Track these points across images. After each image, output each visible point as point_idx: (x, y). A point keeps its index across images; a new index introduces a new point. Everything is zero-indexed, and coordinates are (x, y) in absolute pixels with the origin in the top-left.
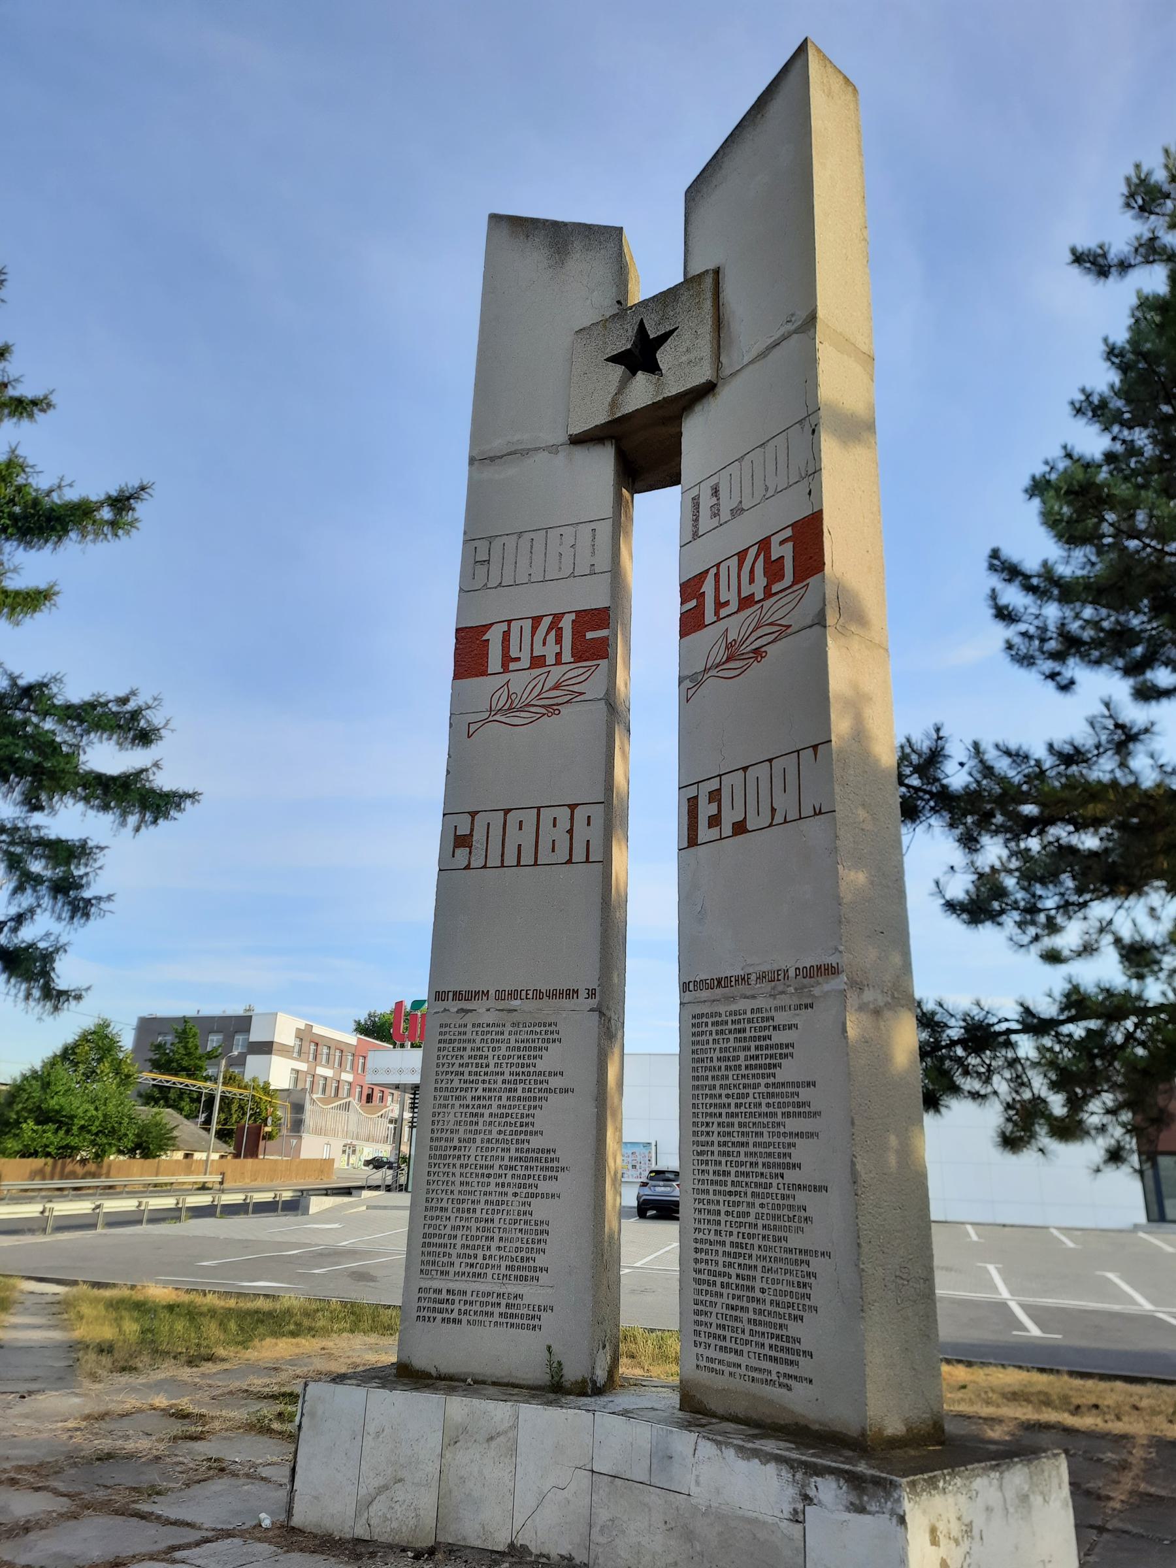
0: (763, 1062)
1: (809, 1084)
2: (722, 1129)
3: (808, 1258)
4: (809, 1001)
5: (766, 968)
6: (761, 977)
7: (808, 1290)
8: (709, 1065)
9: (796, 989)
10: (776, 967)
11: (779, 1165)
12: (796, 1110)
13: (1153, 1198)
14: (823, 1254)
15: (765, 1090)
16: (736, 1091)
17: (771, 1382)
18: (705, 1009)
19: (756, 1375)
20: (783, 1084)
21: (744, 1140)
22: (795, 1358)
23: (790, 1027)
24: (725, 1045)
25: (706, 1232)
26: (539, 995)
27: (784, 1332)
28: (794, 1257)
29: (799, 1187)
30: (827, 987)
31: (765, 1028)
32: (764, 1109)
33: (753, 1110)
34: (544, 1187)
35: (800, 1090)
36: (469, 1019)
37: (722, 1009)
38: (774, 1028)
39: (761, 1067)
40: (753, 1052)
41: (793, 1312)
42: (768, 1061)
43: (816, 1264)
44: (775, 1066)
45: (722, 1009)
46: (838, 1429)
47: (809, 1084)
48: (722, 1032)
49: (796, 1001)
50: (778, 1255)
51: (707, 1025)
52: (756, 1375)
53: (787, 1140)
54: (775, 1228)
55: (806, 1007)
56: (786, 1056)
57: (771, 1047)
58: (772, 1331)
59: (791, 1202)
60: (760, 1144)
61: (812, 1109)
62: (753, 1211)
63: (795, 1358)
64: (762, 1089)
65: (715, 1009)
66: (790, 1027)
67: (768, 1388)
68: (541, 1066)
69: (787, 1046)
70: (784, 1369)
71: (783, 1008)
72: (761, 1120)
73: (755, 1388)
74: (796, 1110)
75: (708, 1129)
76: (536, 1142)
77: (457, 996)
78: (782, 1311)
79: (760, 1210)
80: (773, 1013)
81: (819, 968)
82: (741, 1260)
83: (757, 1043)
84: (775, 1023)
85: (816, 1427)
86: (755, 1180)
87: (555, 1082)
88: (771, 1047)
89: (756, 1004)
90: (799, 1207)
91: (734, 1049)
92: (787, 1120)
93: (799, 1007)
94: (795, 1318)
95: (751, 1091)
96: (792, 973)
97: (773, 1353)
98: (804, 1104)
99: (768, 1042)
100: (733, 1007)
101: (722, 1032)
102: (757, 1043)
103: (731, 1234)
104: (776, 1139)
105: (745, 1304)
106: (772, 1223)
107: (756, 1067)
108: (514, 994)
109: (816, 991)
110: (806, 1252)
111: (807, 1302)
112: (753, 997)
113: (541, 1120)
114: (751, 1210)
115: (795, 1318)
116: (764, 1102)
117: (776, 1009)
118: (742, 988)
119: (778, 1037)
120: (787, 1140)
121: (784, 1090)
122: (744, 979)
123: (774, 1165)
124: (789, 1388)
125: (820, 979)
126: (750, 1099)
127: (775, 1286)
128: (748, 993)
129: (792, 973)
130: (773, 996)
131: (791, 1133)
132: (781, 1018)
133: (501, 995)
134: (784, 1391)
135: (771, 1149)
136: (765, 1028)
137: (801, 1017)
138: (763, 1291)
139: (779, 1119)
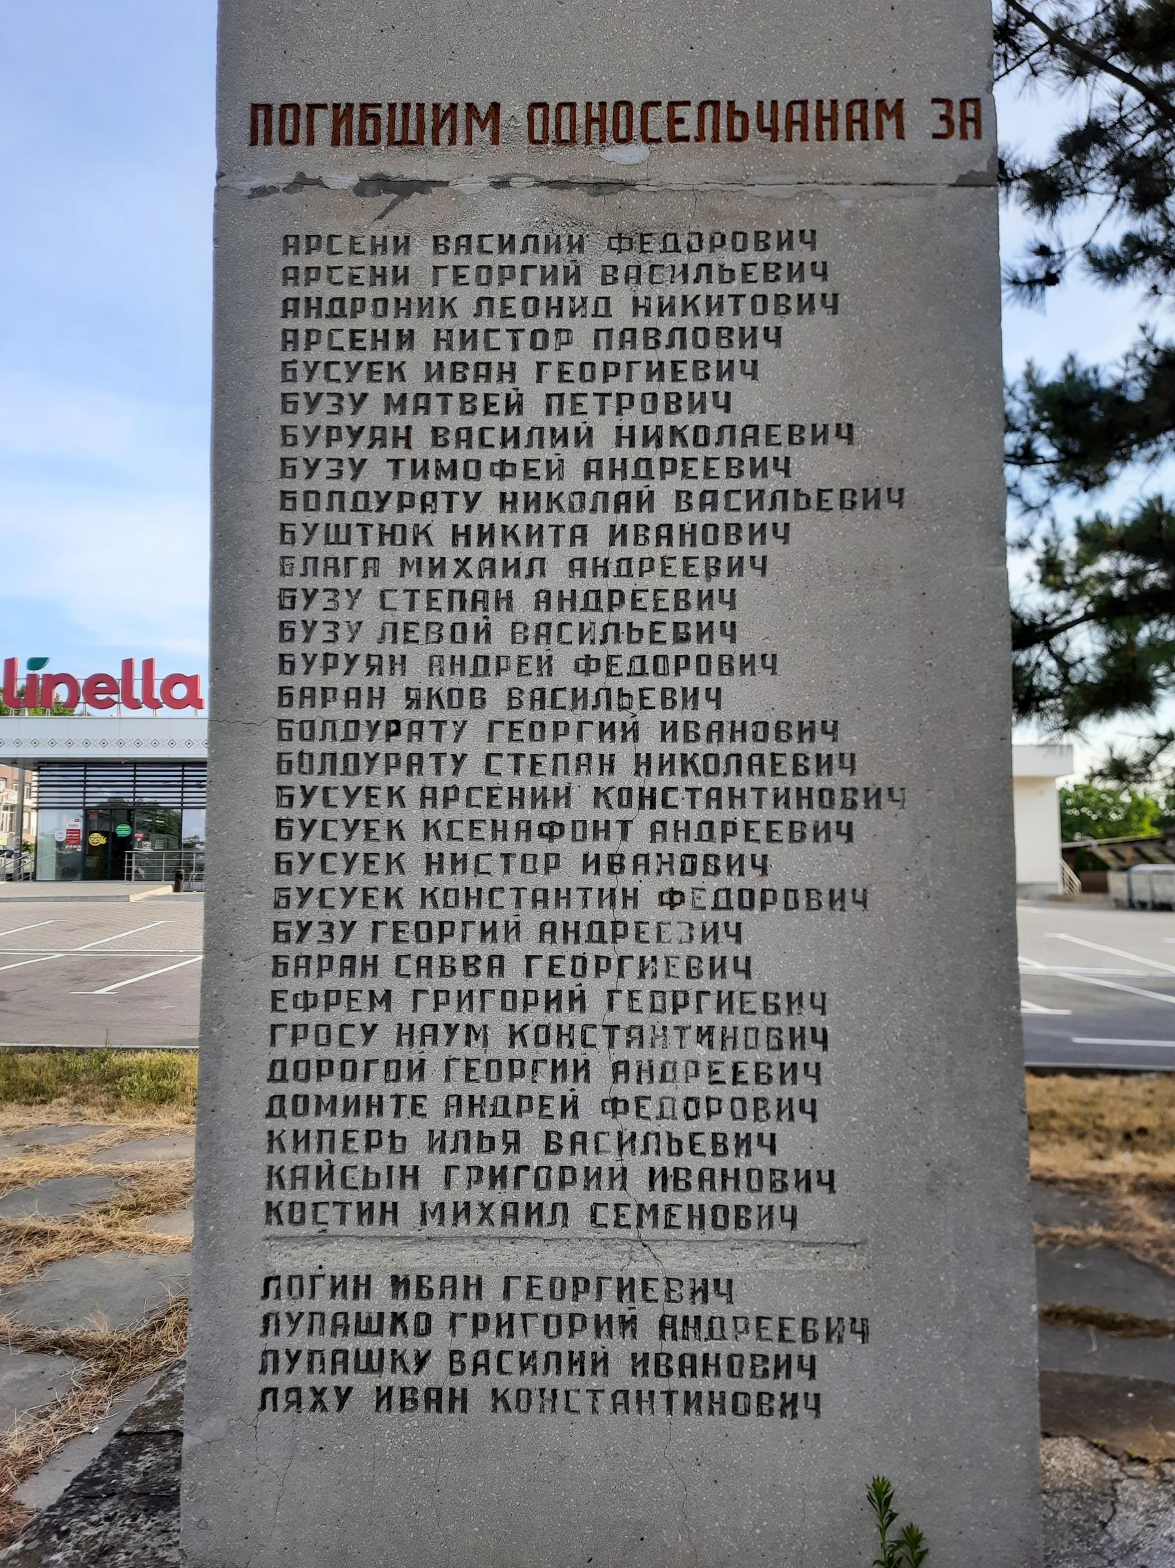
26: (726, 122)
34: (792, 864)
36: (414, 215)
68: (752, 403)
76: (745, 697)
77: (355, 123)
87: (814, 467)
108: (614, 121)
113: (760, 611)
133: (551, 124)
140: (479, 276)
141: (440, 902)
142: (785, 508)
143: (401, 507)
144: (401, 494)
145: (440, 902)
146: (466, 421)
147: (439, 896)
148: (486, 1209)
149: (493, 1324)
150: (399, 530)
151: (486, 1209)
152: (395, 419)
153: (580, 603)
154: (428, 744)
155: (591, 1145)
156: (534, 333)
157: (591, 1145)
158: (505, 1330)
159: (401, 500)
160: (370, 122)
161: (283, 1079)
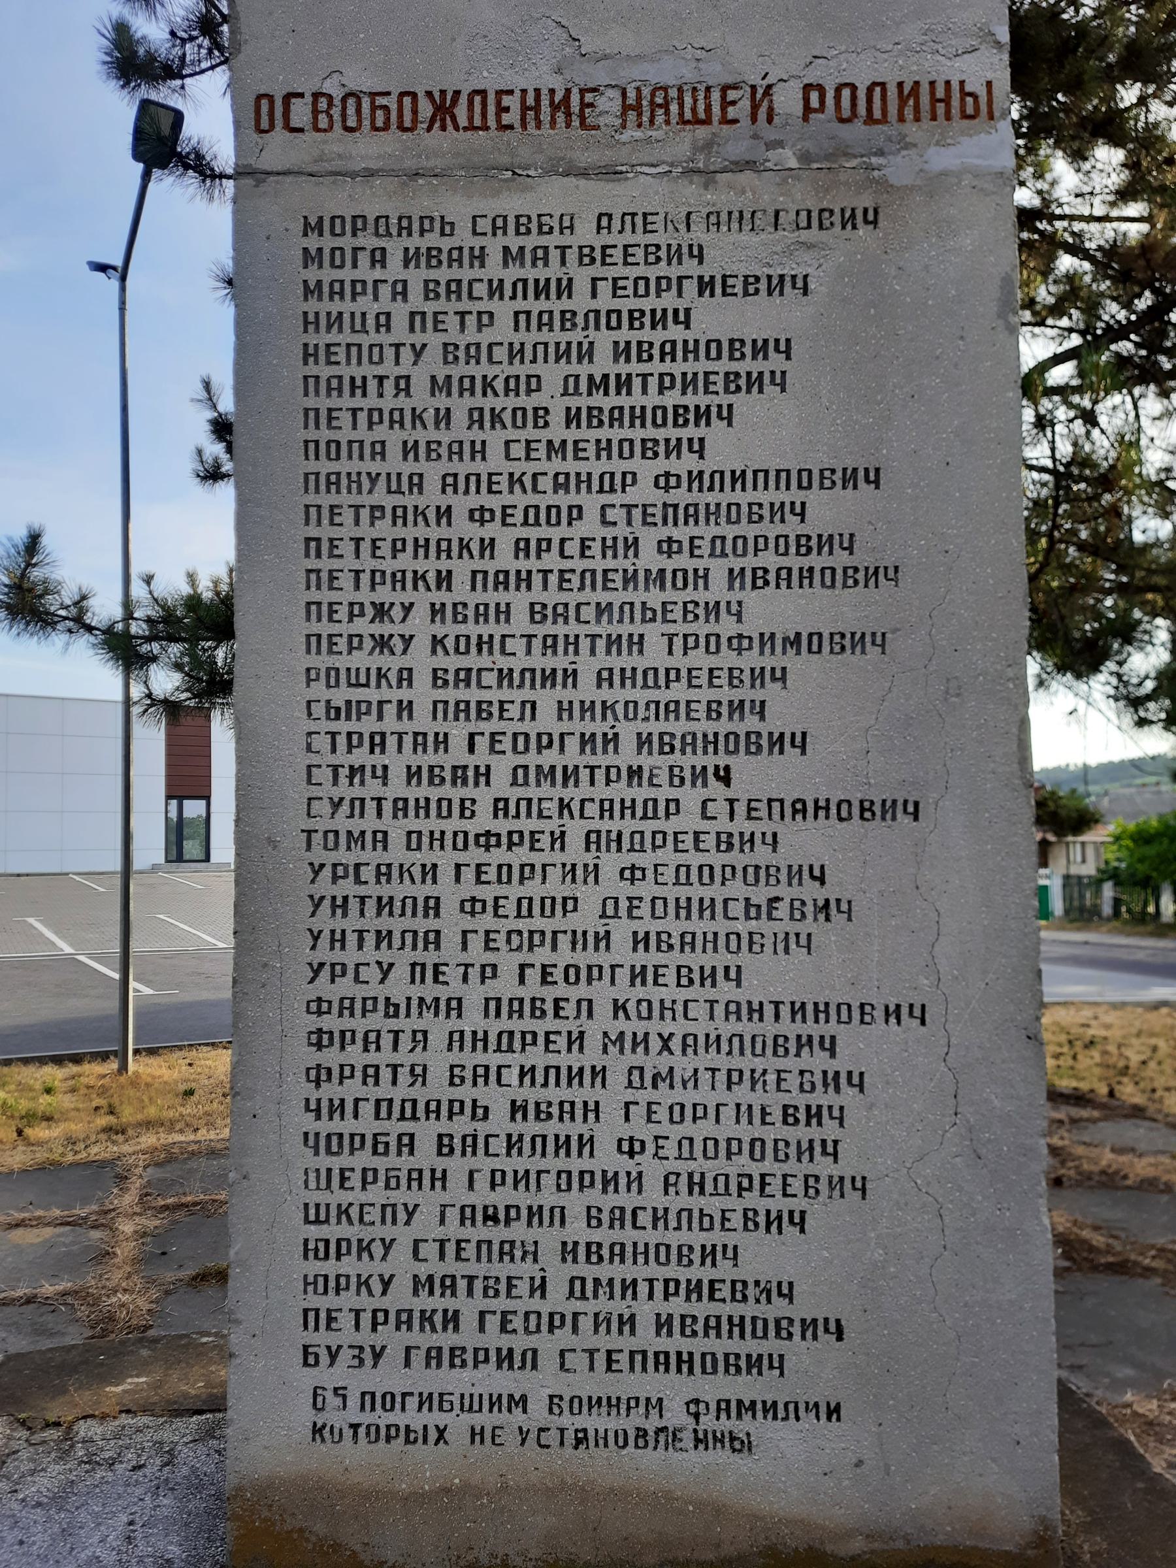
0: (652, 399)
1: (850, 478)
2: (450, 630)
3: (832, 1028)
4: (866, 201)
5: (669, 72)
6: (646, 105)
7: (830, 1130)
8: (388, 403)
9: (805, 158)
10: (715, 73)
11: (712, 742)
12: (795, 562)
13: (173, 838)
14: (893, 1013)
15: (658, 497)
16: (520, 499)
17: (669, 1437)
18: (375, 201)
19: (595, 1422)
20: (738, 478)
21: (560, 662)
22: (771, 1345)
23: (776, 285)
24: (471, 335)
25: (371, 974)
27: (725, 1270)
28: (769, 1028)
29: (799, 808)
30: (941, 159)
31: (662, 285)
32: (649, 559)
33: (599, 565)
35: (814, 497)
37: (458, 207)
38: (705, 286)
39: (638, 416)
40: (603, 364)
41: (762, 1204)
42: (672, 398)
43: (858, 1046)
44: (703, 415)
45: (458, 207)
46: (939, 1540)
47: (850, 478)
48: (454, 289)
49: (802, 196)
50: (701, 1028)
51: (379, 258)
52: (595, 1422)
53: (751, 659)
54: (688, 942)
55: (849, 220)
56: (755, 382)
57: (691, 350)
58: (672, 1271)
59: (762, 855)
60: (627, 677)
61: (863, 558)
62: (590, 897)
63: (771, 1345)
64: (644, 492)
65: (422, 203)
66: (776, 285)
67: (651, 1459)
69: (761, 349)
70: (744, 1387)
71: (743, 219)
72: (637, 597)
73: (597, 1465)
74: (795, 562)
75: (385, 629)
78: (713, 1205)
79: (624, 890)
80: (699, 234)
81: (909, 94)
82: (536, 1057)
83: (624, 334)
84: (706, 271)
85: (857, 1545)
86: (601, 791)
88: (691, 350)
89: (618, 197)
90: (795, 874)
91: (516, 353)
92: (751, 598)
93: (820, 218)
94: (774, 1222)
95: (591, 503)
96: (788, 100)
97: (675, 1343)
98: (826, 542)
99: (676, 332)
100: (512, 204)
101: (454, 289)
102: (624, 334)
103: (489, 972)
104: (699, 659)
105: (548, 1198)
106: (674, 927)
107: (616, 416)
109: (898, 169)
110: (821, 1011)
111: (823, 1166)
112: (611, 173)
114: (580, 891)
115: (774, 1222)
116: (649, 538)
117: (714, 220)
118: (556, 138)
119: (713, 319)
120: (751, 659)
121: (743, 498)
122: (569, 107)
123: (689, 742)
124: (741, 1445)
125: (912, 130)
126: (589, 526)
127: (687, 1129)
128: (585, 158)
129: (788, 100)
130: (708, 176)
131: (767, 641)
132: (730, 253)
134: (721, 1456)
135: (679, 692)
136: (662, 285)
137: (828, 259)
138: (631, 1148)
139: (718, 590)
140: (509, 941)
141: (576, 814)
142: (594, 587)
143: (335, 878)
144: (335, 866)
145: (576, 814)
146: (564, 597)
147: (620, 709)
148: (666, 1041)
149: (493, 1358)
150: (321, 1280)
151: (666, 1041)
152: (426, 856)
153: (492, 1045)
154: (385, 1057)
155: (493, 1077)
156: (636, 280)
157: (493, 1077)
158: (707, 913)
159: (334, 873)
160: (379, 113)
161: (612, 490)
